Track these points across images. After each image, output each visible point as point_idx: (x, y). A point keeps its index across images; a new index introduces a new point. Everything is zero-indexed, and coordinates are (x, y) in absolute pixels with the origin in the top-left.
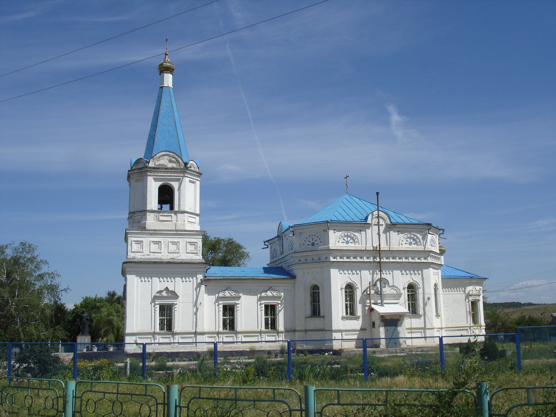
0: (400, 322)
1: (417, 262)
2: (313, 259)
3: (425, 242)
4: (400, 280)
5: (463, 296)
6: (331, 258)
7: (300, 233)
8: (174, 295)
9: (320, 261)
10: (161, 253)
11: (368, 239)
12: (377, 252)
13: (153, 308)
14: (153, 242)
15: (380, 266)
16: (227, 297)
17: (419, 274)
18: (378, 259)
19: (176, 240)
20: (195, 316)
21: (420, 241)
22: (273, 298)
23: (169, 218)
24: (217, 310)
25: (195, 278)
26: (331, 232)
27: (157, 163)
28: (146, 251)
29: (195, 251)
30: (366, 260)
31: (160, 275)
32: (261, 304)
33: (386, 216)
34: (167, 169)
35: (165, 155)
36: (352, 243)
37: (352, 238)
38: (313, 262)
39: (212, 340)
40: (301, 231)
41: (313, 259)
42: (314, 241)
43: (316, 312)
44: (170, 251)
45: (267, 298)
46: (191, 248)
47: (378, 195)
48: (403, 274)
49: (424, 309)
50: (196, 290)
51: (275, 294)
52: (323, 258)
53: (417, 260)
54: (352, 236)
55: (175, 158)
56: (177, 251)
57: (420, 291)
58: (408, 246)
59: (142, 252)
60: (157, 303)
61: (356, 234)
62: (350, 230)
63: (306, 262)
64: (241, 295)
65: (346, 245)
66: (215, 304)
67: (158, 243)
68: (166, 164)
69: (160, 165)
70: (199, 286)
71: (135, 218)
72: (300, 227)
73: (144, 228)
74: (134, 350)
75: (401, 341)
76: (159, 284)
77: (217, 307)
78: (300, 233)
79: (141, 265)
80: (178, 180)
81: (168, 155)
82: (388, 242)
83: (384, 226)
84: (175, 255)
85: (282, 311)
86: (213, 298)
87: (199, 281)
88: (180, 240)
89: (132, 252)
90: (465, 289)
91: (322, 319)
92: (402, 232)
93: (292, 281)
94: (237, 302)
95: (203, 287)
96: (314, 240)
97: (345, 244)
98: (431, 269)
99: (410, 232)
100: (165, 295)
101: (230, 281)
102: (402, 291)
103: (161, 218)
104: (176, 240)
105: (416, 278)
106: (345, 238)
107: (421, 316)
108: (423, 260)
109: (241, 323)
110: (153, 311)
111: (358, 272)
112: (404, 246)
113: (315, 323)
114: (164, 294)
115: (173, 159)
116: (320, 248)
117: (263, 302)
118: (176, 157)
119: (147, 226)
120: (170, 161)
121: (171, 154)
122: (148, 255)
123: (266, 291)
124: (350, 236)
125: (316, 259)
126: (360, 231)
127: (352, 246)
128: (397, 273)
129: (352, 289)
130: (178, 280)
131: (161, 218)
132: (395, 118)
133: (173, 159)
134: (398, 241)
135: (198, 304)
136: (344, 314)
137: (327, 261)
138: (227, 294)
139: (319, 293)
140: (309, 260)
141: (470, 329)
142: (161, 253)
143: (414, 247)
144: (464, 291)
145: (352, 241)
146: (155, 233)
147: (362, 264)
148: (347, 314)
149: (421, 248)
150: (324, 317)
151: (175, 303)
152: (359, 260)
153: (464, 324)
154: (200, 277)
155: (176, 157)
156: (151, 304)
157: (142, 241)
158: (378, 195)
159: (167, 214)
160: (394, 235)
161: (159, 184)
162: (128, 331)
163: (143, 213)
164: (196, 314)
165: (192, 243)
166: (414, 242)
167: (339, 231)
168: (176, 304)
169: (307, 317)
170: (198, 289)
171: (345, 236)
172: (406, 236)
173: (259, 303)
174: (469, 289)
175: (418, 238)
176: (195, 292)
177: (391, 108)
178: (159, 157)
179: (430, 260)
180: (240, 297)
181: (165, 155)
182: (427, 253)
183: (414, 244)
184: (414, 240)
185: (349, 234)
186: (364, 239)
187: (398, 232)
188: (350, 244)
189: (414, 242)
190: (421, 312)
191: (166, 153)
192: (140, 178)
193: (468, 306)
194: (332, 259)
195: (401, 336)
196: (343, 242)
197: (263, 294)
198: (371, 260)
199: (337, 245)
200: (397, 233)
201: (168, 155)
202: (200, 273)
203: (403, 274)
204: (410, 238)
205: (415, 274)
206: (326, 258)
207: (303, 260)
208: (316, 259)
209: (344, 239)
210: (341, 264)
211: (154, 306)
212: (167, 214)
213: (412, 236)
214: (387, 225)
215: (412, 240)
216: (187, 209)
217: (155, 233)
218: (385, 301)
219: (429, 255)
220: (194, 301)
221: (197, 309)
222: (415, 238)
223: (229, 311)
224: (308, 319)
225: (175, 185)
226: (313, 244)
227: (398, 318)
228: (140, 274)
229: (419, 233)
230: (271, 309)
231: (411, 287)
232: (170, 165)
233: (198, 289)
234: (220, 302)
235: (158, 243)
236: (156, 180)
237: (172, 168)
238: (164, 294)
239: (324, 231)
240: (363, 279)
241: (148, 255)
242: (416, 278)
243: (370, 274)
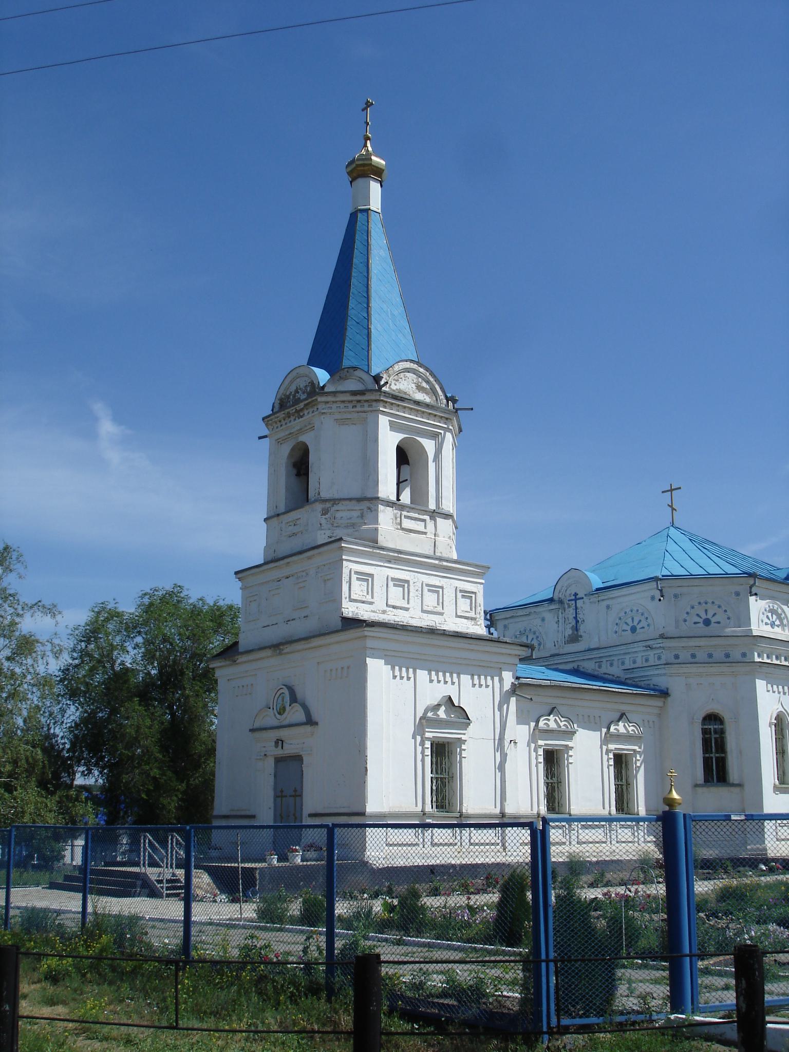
2: (710, 656)
7: (676, 596)
8: (461, 717)
9: (727, 659)
10: (407, 609)
13: (419, 749)
14: (393, 579)
16: (552, 731)
20: (498, 774)
23: (419, 526)
24: (534, 762)
25: (496, 679)
28: (380, 604)
29: (472, 614)
31: (435, 665)
32: (608, 751)
35: (407, 370)
37: (779, 617)
38: (710, 660)
40: (678, 591)
41: (710, 656)
43: (716, 769)
44: (425, 608)
45: (618, 738)
46: (464, 605)
50: (500, 709)
52: (736, 655)
54: (780, 611)
55: (428, 382)
56: (439, 609)
59: (371, 603)
60: (428, 735)
63: (693, 660)
65: (772, 630)
66: (529, 745)
67: (402, 583)
69: (400, 391)
70: (505, 699)
71: (338, 515)
72: (679, 583)
73: (372, 540)
76: (431, 688)
77: (533, 754)
78: (676, 596)
79: (402, 636)
80: (434, 436)
87: (507, 686)
89: (351, 600)
91: (736, 790)
93: (658, 702)
95: (513, 700)
97: (769, 628)
103: (407, 524)
110: (419, 757)
113: (713, 800)
116: (729, 631)
117: (612, 747)
118: (432, 379)
119: (380, 539)
120: (420, 388)
121: (421, 370)
122: (384, 612)
125: (718, 655)
130: (466, 679)
131: (407, 524)
132: (107, 427)
133: (424, 385)
135: (506, 743)
137: (744, 660)
139: (722, 732)
140: (701, 656)
146: (397, 557)
150: (740, 785)
151: (463, 737)
154: (508, 678)
155: (432, 379)
157: (372, 576)
159: (416, 515)
162: (215, 813)
163: (367, 504)
164: (501, 768)
165: (467, 595)
169: (696, 786)
170: (505, 706)
173: (604, 748)
176: (497, 713)
177: (99, 408)
178: (400, 372)
180: (570, 734)
181: (407, 370)
188: (777, 629)
191: (415, 366)
192: (355, 415)
196: (766, 624)
202: (511, 667)
206: (744, 655)
207: (685, 656)
208: (718, 655)
210: (771, 670)
212: (416, 515)
217: (397, 557)
220: (497, 738)
221: (504, 757)
223: (553, 761)
224: (699, 790)
225: (429, 446)
226: (707, 622)
228: (393, 659)
233: (505, 706)
234: (541, 742)
235: (402, 583)
236: (394, 427)
238: (442, 713)
239: (737, 594)
241: (384, 612)
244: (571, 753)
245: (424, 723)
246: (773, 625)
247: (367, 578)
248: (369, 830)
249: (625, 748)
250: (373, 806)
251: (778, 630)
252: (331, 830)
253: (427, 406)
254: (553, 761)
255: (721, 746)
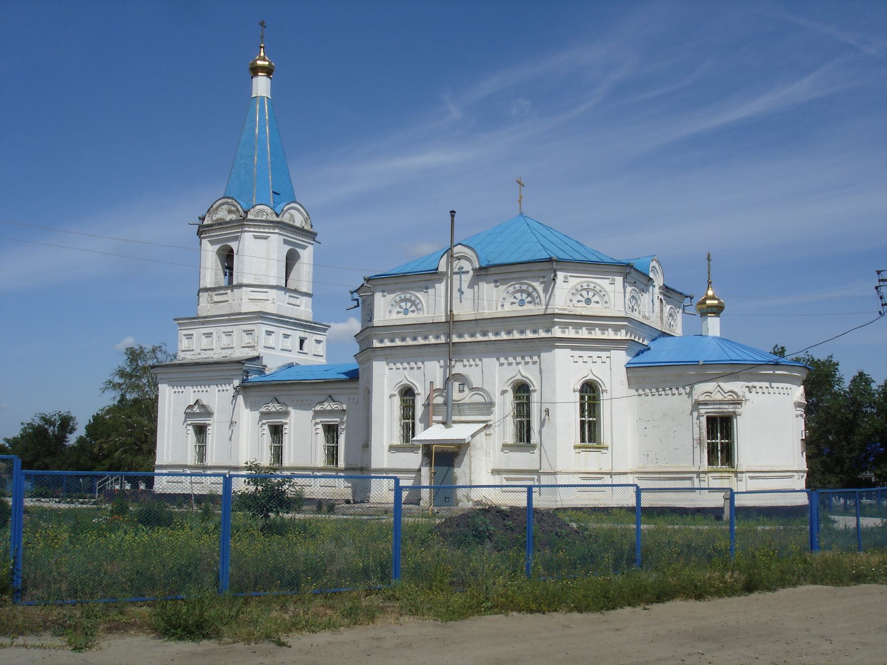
0: (459, 457)
1: (531, 337)
3: (548, 296)
4: (494, 376)
5: (688, 404)
6: (375, 341)
10: (212, 349)
11: (431, 305)
12: (451, 324)
15: (451, 352)
17: (535, 363)
18: (451, 340)
19: (229, 329)
21: (539, 297)
22: (332, 413)
26: (378, 296)
27: (214, 219)
30: (432, 340)
31: (194, 382)
33: (474, 254)
34: (227, 223)
36: (413, 311)
37: (413, 303)
39: (725, 484)
42: (583, 299)
47: (453, 216)
48: (502, 365)
49: (540, 432)
51: (334, 406)
53: (529, 335)
54: (413, 298)
55: (234, 206)
57: (535, 397)
58: (516, 307)
61: (418, 294)
62: (409, 289)
64: (290, 409)
68: (224, 217)
69: (217, 220)
74: (163, 489)
75: (460, 493)
76: (191, 394)
79: (210, 368)
81: (226, 203)
82: (476, 301)
83: (471, 273)
84: (229, 352)
85: (344, 432)
86: (257, 414)
88: (234, 329)
90: (692, 389)
92: (504, 281)
94: (284, 421)
95: (240, 398)
96: (580, 298)
97: (401, 316)
98: (557, 351)
99: (402, 290)
100: (198, 411)
101: (274, 388)
102: (497, 399)
104: (229, 329)
105: (527, 372)
106: (584, 293)
107: (534, 447)
108: (542, 334)
109: (747, 450)
111: (535, 358)
112: (394, 316)
114: (196, 409)
115: (233, 208)
118: (235, 203)
120: (230, 212)
122: (199, 354)
123: (321, 403)
124: (409, 300)
126: (427, 288)
127: (413, 317)
128: (490, 363)
129: (594, 392)
130: (214, 389)
131: (216, 298)
133: (233, 208)
134: (495, 300)
136: (578, 441)
138: (327, 406)
141: (698, 477)
142: (212, 349)
143: (530, 309)
144: (690, 394)
145: (413, 308)
147: (427, 349)
148: (583, 440)
149: (539, 310)
152: (421, 341)
153: (686, 466)
154: (237, 383)
156: (691, 414)
158: (453, 216)
160: (487, 288)
161: (218, 247)
166: (529, 299)
167: (391, 292)
168: (209, 425)
171: (402, 301)
172: (511, 289)
174: (702, 389)
175: (535, 289)
179: (557, 332)
180: (286, 414)
182: (549, 319)
183: (530, 302)
184: (529, 295)
185: (408, 296)
186: (432, 302)
187: (496, 281)
188: (410, 315)
189: (529, 299)
190: (535, 439)
191: (226, 200)
193: (696, 429)
194: (376, 344)
195: (460, 483)
196: (398, 312)
197: (318, 408)
198: (442, 340)
199: (387, 318)
200: (493, 285)
201: (226, 203)
203: (502, 365)
204: (522, 291)
205: (527, 363)
209: (401, 307)
211: (698, 418)
213: (524, 287)
214: (474, 270)
215: (525, 296)
216: (245, 282)
218: (455, 418)
219: (554, 324)
222: (530, 289)
225: (233, 245)
227: (456, 450)
228: (172, 383)
229: (535, 278)
230: (721, 424)
231: (522, 389)
232: (228, 217)
236: (212, 243)
237: (231, 221)
240: (427, 375)
242: (527, 372)
243: (441, 367)
244: (285, 427)
245: (189, 414)
246: (522, 303)
247: (189, 337)
248: (373, 480)
249: (333, 420)
250: (375, 465)
251: (528, 307)
252: (530, 489)
253: (236, 221)
254: (277, 431)
255: (405, 416)
